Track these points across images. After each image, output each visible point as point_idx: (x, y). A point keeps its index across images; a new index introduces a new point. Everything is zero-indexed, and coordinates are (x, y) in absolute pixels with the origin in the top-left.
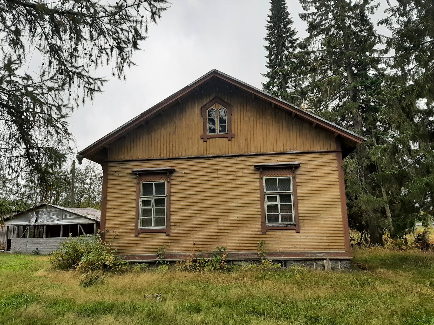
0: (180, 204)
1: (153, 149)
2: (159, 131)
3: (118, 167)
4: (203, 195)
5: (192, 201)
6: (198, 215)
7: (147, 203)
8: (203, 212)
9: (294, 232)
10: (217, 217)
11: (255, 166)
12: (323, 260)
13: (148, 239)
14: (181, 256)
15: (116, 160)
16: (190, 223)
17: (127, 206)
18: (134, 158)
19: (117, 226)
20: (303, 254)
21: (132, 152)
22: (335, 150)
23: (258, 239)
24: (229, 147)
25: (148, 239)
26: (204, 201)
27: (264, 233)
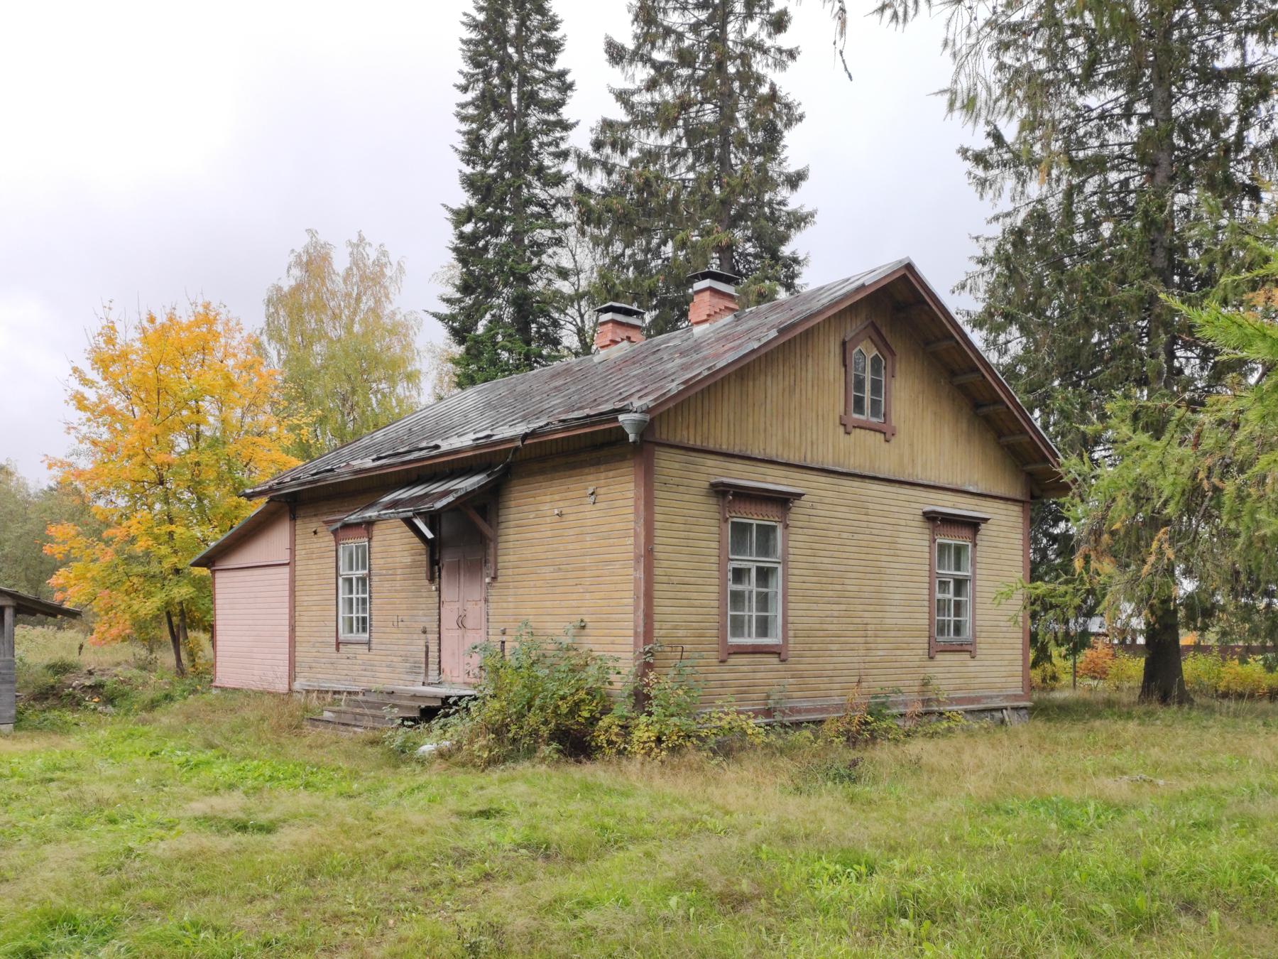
0: (805, 586)
1: (751, 427)
2: (763, 378)
3: (677, 465)
4: (843, 568)
5: (824, 580)
6: (836, 614)
7: (739, 575)
8: (843, 607)
9: (966, 656)
10: (865, 621)
11: (713, 485)
12: (1001, 709)
13: (745, 668)
14: (808, 711)
15: (672, 441)
16: (821, 633)
17: (700, 581)
18: (711, 446)
19: (681, 633)
20: (977, 700)
21: (706, 425)
22: (1018, 497)
23: (922, 670)
24: (886, 459)
25: (745, 668)
26: (847, 581)
27: (931, 658)
